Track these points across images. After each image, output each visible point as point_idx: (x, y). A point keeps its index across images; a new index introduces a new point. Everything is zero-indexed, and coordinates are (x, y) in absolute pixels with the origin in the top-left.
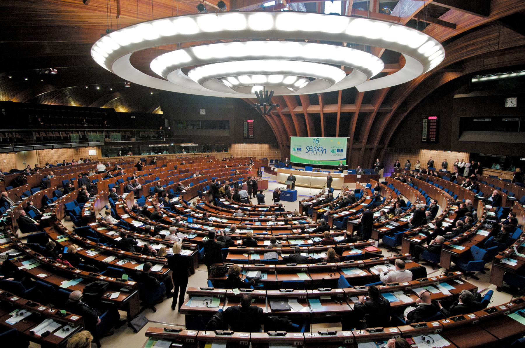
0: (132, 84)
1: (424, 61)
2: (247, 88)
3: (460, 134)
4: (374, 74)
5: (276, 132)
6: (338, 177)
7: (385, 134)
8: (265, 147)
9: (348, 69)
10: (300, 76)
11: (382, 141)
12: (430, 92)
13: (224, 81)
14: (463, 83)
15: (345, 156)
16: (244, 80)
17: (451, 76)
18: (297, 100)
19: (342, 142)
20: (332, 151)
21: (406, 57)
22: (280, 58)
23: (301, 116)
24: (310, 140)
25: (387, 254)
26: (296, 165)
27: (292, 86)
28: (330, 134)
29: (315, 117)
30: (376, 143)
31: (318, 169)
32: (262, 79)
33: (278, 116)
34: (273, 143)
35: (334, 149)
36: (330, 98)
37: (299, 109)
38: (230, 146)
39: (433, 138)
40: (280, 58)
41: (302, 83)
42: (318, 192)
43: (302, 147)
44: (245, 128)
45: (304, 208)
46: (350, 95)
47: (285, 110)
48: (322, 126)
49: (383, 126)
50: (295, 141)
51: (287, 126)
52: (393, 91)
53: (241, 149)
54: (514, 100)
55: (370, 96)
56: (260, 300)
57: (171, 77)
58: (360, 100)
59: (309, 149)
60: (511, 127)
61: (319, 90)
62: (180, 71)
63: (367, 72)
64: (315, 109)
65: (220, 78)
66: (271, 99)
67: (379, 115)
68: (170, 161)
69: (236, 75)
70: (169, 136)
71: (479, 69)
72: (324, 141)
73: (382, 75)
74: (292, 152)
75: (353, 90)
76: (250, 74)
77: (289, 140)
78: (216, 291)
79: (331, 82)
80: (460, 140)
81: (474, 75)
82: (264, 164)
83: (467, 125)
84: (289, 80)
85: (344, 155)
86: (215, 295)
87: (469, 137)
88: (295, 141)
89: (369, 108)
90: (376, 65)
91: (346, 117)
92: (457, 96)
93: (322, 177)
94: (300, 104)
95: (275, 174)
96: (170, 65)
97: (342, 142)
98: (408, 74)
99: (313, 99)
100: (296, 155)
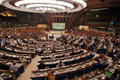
0: (8, 8)
1: (83, 6)
2: (42, 11)
3: (87, 22)
4: (72, 8)
5: (49, 22)
6: (63, 32)
7: (73, 22)
8: (46, 25)
9: (66, 7)
10: (55, 8)
11: (72, 24)
12: (83, 12)
13: (36, 9)
14: (88, 11)
15: (65, 27)
16: (41, 9)
17: (86, 10)
18: (53, 14)
19: (64, 24)
20: (62, 26)
21: (79, 6)
22: (51, 4)
23: (55, 18)
24: (57, 24)
25: (70, 46)
26: (54, 30)
27: (53, 11)
28: (61, 22)
29: (58, 18)
30: (71, 24)
31: (58, 30)
32: (46, 9)
33: (52, 18)
34: (48, 24)
35: (62, 26)
36: (61, 14)
37: (54, 16)
38: (37, 25)
39: (82, 23)
40: (51, 4)
41: (64, 8)
42: (60, 36)
43: (55, 25)
44: (41, 21)
45: (57, 40)
46: (66, 13)
47: (51, 16)
48: (59, 21)
49: (71, 20)
50: (54, 24)
51: (51, 20)
52: (75, 13)
53: (40, 26)
54: (98, 16)
55: (70, 13)
56: (45, 62)
57: (21, 7)
58: (68, 14)
59: (57, 26)
60: (97, 21)
61: (59, 12)
62: (23, 6)
63: (70, 8)
64: (58, 16)
65: (35, 8)
66: (47, 13)
67: (72, 18)
68: (21, 29)
69: (39, 7)
70: (20, 23)
71: (92, 8)
72: (60, 24)
73: (73, 9)
74: (53, 27)
75: (67, 12)
76: (43, 7)
77: (52, 24)
78: (41, 70)
79: (62, 10)
80: (88, 23)
81: (91, 9)
82: (47, 30)
83: (89, 20)
84: (53, 9)
85: (64, 27)
86: (41, 72)
87: (89, 23)
88: (54, 24)
89: (65, 16)
90: (72, 6)
91: (65, 18)
92: (87, 14)
93: (60, 32)
94: (54, 15)
95: (49, 32)
96: (21, 4)
97: (64, 24)
98: (79, 9)
99: (57, 14)
100: (54, 27)
